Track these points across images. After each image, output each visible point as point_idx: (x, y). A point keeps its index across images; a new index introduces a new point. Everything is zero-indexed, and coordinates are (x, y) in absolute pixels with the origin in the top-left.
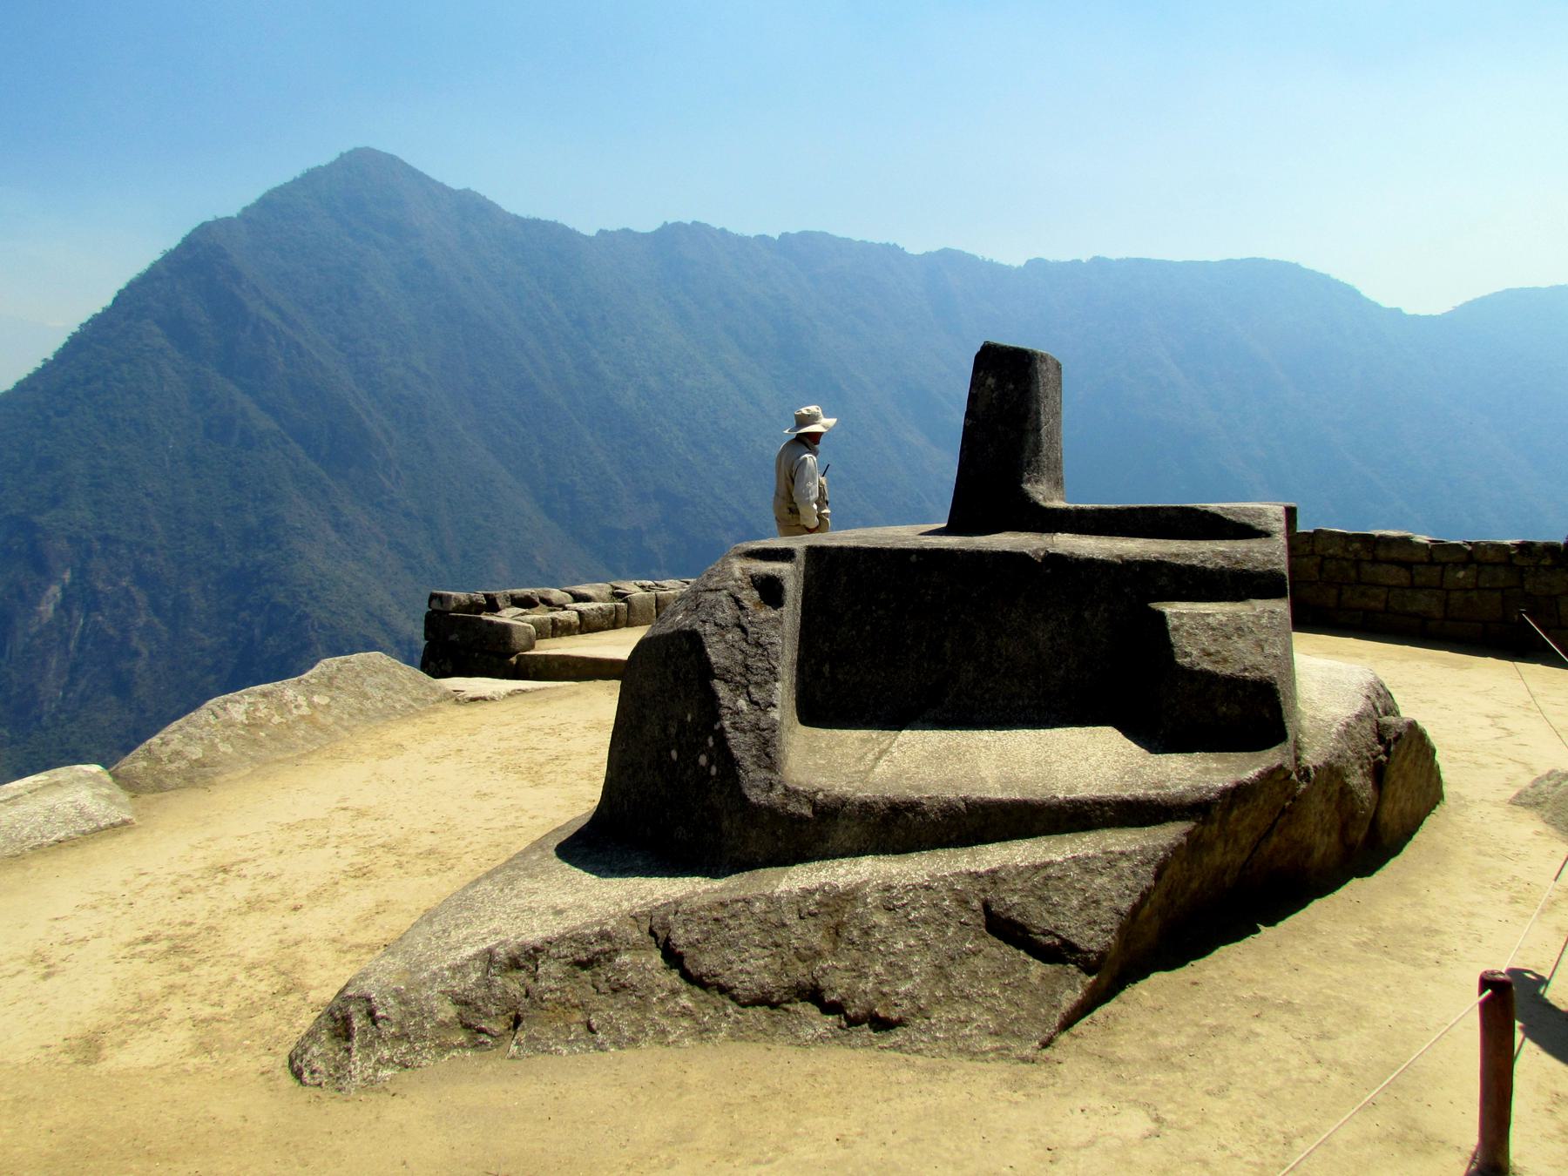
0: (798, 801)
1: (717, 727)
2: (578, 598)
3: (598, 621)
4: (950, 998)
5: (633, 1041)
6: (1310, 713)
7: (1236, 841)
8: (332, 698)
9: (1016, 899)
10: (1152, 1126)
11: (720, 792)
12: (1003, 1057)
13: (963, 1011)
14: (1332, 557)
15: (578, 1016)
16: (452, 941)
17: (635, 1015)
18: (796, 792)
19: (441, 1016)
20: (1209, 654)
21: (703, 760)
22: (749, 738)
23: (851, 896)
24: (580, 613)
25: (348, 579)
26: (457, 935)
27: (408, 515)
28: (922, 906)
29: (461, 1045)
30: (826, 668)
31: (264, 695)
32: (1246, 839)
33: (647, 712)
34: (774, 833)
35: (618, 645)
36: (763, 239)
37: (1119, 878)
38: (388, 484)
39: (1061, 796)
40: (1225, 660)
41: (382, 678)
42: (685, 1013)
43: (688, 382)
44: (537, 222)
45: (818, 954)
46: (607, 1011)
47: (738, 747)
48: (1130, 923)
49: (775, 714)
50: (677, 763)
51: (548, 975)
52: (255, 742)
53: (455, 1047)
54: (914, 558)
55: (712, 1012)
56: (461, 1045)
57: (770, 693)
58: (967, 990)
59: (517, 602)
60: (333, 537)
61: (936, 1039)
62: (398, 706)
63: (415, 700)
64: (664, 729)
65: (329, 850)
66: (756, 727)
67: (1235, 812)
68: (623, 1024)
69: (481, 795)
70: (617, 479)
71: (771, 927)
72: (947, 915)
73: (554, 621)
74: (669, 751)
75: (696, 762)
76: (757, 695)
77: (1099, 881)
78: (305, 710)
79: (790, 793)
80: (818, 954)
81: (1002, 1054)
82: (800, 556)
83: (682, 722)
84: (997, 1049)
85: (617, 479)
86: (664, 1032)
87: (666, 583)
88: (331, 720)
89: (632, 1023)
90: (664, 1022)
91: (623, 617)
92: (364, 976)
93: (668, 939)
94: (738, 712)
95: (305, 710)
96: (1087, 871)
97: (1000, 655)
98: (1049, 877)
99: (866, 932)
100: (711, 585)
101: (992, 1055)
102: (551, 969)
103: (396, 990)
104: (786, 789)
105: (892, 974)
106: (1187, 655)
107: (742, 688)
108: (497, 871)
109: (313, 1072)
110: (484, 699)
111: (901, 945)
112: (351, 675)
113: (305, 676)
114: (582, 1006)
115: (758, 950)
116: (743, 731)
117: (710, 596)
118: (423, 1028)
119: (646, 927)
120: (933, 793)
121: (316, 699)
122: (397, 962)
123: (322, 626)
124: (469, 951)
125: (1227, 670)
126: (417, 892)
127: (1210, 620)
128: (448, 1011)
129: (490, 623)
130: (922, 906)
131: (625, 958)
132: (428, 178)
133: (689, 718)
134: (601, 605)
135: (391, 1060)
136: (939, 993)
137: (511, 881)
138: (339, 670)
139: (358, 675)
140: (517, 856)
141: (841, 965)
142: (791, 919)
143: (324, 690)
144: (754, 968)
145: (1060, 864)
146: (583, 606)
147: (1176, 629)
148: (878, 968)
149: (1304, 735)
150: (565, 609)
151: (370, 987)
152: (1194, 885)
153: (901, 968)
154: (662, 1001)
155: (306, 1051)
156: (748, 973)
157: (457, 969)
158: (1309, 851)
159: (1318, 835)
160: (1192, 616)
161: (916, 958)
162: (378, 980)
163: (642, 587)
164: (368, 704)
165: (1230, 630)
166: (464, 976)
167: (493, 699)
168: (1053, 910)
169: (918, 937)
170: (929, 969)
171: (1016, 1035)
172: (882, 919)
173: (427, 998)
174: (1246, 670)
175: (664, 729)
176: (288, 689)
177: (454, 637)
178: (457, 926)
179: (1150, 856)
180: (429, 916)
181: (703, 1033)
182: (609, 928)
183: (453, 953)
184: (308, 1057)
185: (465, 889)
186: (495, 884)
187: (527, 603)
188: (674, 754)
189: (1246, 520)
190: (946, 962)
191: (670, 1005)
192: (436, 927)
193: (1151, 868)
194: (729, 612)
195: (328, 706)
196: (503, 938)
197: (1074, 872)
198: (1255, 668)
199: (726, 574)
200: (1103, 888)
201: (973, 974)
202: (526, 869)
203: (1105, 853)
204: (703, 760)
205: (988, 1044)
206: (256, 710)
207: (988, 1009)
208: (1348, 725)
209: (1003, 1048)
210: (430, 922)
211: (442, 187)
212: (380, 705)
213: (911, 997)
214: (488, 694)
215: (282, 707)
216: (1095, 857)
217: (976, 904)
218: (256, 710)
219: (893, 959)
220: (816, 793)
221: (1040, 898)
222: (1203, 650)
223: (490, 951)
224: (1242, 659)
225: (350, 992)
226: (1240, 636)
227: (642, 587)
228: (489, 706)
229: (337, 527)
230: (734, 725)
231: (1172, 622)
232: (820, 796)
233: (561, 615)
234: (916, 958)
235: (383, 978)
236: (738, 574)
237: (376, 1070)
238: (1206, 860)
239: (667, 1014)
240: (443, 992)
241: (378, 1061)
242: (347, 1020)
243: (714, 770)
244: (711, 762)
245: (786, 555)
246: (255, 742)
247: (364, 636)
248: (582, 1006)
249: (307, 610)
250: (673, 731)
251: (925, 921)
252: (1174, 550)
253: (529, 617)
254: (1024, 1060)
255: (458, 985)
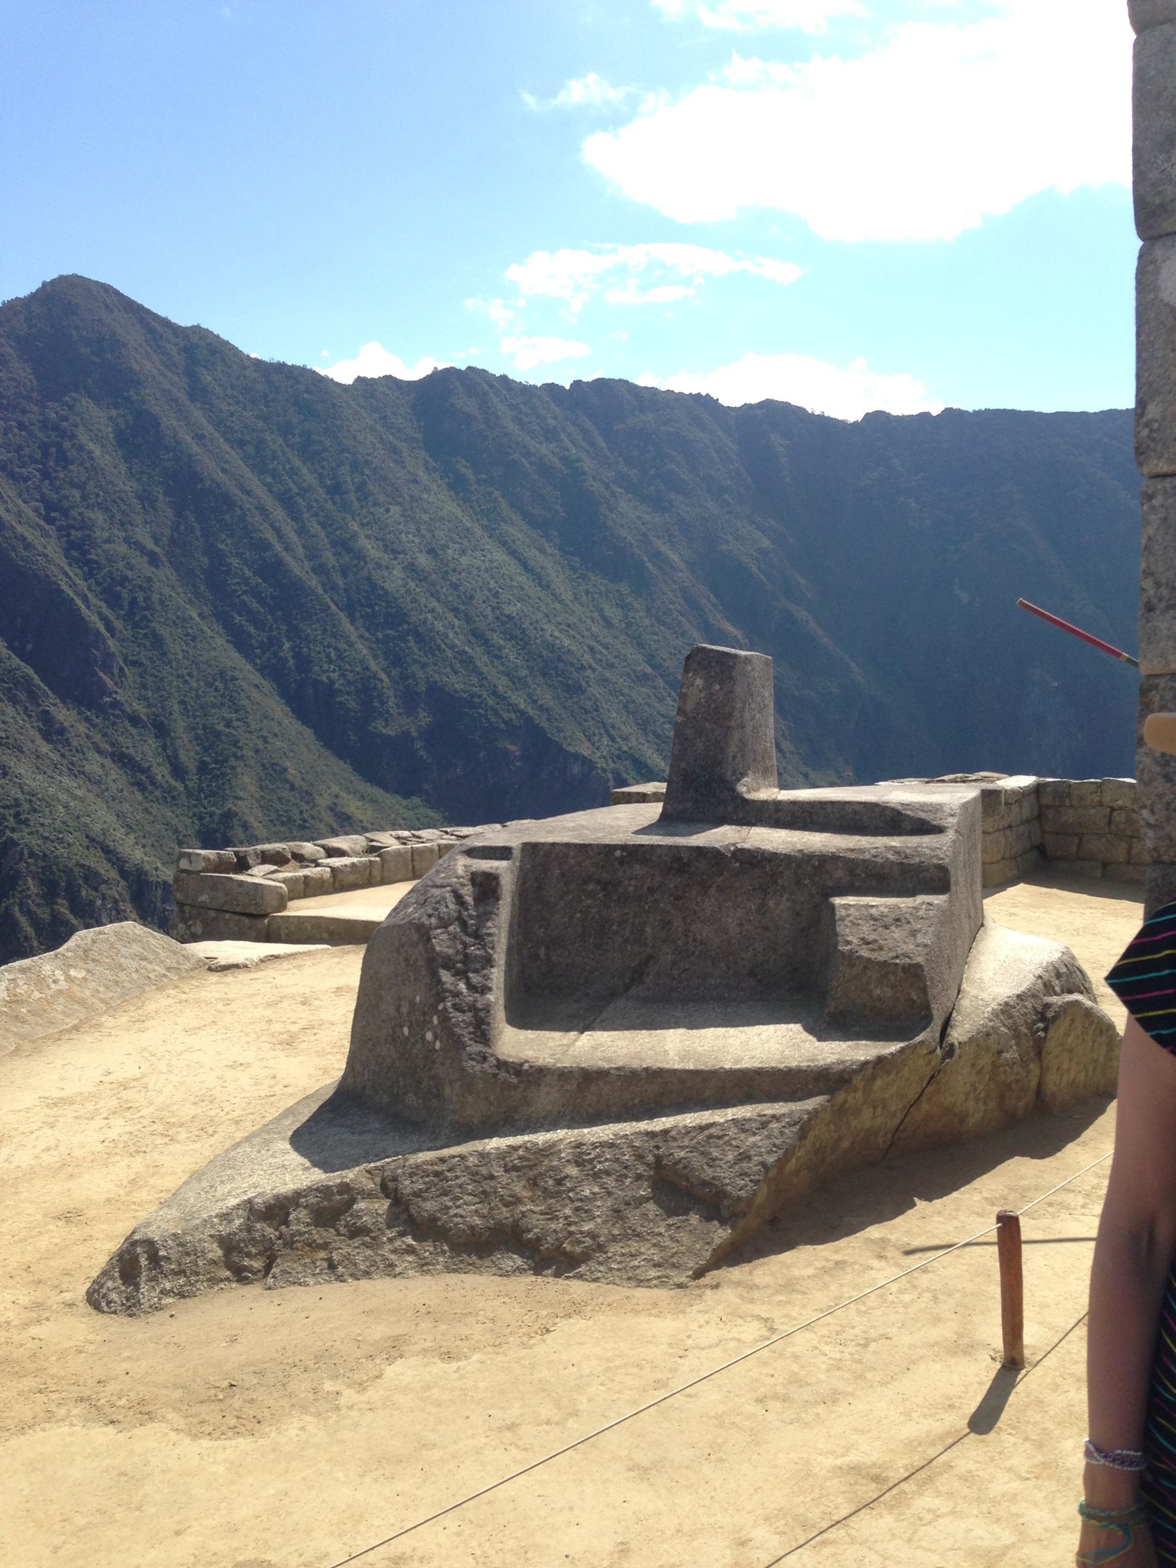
0: (508, 1072)
1: (440, 1007)
2: (332, 852)
3: (352, 878)
4: (625, 1237)
5: (367, 1274)
6: (973, 992)
7: (884, 1107)
8: (88, 971)
9: (682, 1154)
10: (765, 1333)
11: (443, 1064)
12: (663, 1285)
13: (634, 1246)
14: (1121, 808)
15: (323, 1254)
16: (218, 1194)
17: (369, 1252)
18: (506, 1063)
19: (210, 1256)
20: (868, 943)
21: (429, 1036)
22: (468, 1017)
23: (549, 1151)
24: (333, 870)
25: (64, 797)
26: (222, 1190)
27: (134, 720)
28: (606, 1160)
29: (227, 1279)
30: (542, 951)
31: (23, 970)
32: (896, 1106)
33: (383, 993)
34: (487, 1099)
35: (374, 905)
36: (552, 389)
37: (768, 1137)
38: (110, 683)
39: (727, 1067)
40: (881, 948)
41: (136, 948)
42: (411, 1250)
43: (464, 560)
44: (281, 367)
45: (518, 1201)
46: (344, 1248)
47: (456, 1025)
48: (774, 1174)
49: (491, 997)
50: (408, 1039)
51: (298, 1219)
52: (17, 1018)
53: (222, 1280)
54: (618, 853)
55: (431, 1249)
56: (227, 1279)
57: (487, 977)
58: (639, 1229)
59: (265, 858)
60: (45, 748)
61: (611, 1269)
62: (152, 976)
63: (168, 969)
64: (398, 1009)
65: (99, 1122)
66: (473, 1008)
67: (879, 1082)
68: (359, 1259)
69: (234, 1066)
70: (383, 676)
71: (481, 1176)
72: (626, 1168)
73: (306, 877)
74: (401, 1027)
75: (423, 1038)
76: (474, 978)
77: (752, 1139)
78: (63, 985)
79: (502, 1065)
80: (518, 1201)
81: (662, 1281)
82: (516, 853)
83: (412, 1004)
84: (659, 1277)
85: (383, 676)
86: (392, 1265)
87: (424, 833)
88: (88, 993)
89: (367, 1258)
90: (392, 1257)
91: (376, 873)
92: (148, 1224)
93: (396, 1189)
94: (458, 994)
95: (63, 985)
96: (744, 1131)
97: (695, 940)
98: (710, 1137)
99: (559, 1182)
100: (439, 882)
101: (655, 1282)
102: (299, 1218)
103: (174, 1235)
104: (498, 1060)
105: (578, 1216)
106: (848, 943)
107: (461, 974)
108: (254, 1135)
109: (109, 1303)
110: (237, 966)
111: (587, 1193)
112: (105, 946)
113: (61, 950)
114: (325, 1246)
115: (470, 1198)
116: (464, 1012)
117: (436, 892)
118: (197, 1266)
119: (378, 1180)
120: (620, 1064)
121: (72, 972)
122: (174, 1213)
123: (32, 854)
124: (233, 1202)
125: (882, 956)
126: (178, 1162)
127: (873, 911)
128: (216, 1252)
129: (241, 884)
130: (606, 1160)
131: (361, 1205)
132: (148, 311)
133: (418, 999)
134: (355, 860)
135: (171, 1291)
136: (616, 1232)
137: (267, 1143)
138: (94, 942)
139: (112, 946)
140: (271, 1122)
141: (537, 1209)
142: (498, 1171)
143: (80, 964)
144: (468, 1213)
145: (721, 1124)
146: (336, 862)
147: (842, 919)
148: (568, 1211)
149: (959, 1013)
150: (318, 865)
151: (154, 1233)
152: (845, 1144)
153: (586, 1211)
154: (390, 1240)
155: (102, 1286)
156: (462, 1216)
157: (225, 1217)
158: (963, 1117)
159: (971, 1103)
160: (858, 907)
161: (599, 1203)
162: (159, 1227)
163: (398, 838)
164: (122, 975)
165: (889, 920)
166: (231, 1221)
167: (246, 966)
168: (712, 1162)
169: (602, 1186)
170: (609, 1213)
171: (674, 1266)
172: (573, 1171)
173: (200, 1240)
174: (897, 957)
175: (398, 1009)
176: (46, 964)
177: (204, 898)
178: (222, 1182)
179: (796, 1119)
180: (197, 1176)
181: (424, 1267)
182: (348, 1180)
183: (220, 1204)
184: (104, 1290)
185: (227, 1151)
186: (253, 1146)
187: (279, 860)
188: (406, 1030)
189: (922, 815)
190: (623, 1207)
191: (398, 1243)
192: (204, 1184)
193: (795, 1129)
194: (452, 906)
195: (85, 979)
196: (259, 1190)
197: (733, 1131)
198: (905, 955)
199: (450, 869)
200: (754, 1145)
201: (644, 1215)
202: (279, 1133)
203: (760, 1116)
204: (429, 1036)
205: (653, 1273)
206: (17, 986)
207: (655, 1245)
208: (1006, 1004)
209: (663, 1277)
210: (199, 1180)
211: (166, 322)
212: (135, 976)
213: (593, 1235)
214: (240, 960)
215: (41, 981)
216: (750, 1120)
217: (650, 1158)
218: (17, 986)
219: (579, 1204)
220: (521, 1064)
221: (702, 1153)
222: (863, 939)
223: (249, 1201)
224: (901, 945)
225: (136, 1237)
226: (897, 926)
227: (398, 838)
228: (243, 977)
229: (47, 736)
230: (454, 1006)
231: (840, 913)
232: (526, 1067)
233: (311, 871)
234: (599, 1203)
235: (163, 1225)
236: (460, 871)
237: (160, 1299)
238: (854, 1123)
239: (394, 1251)
240: (211, 1236)
241: (161, 1292)
242: (135, 1259)
243: (438, 1045)
244: (436, 1038)
245: (503, 853)
246: (17, 1018)
247: (83, 866)
248: (325, 1246)
249: (15, 836)
250: (404, 1010)
251: (607, 1173)
252: (851, 845)
253: (281, 876)
254: (680, 1286)
255: (224, 1229)
